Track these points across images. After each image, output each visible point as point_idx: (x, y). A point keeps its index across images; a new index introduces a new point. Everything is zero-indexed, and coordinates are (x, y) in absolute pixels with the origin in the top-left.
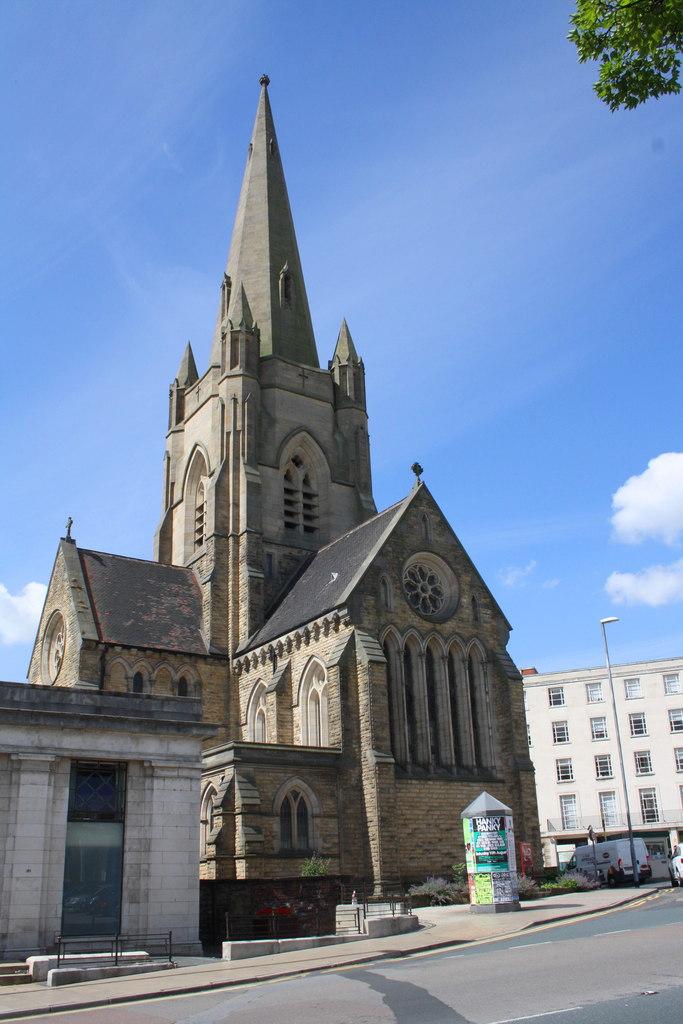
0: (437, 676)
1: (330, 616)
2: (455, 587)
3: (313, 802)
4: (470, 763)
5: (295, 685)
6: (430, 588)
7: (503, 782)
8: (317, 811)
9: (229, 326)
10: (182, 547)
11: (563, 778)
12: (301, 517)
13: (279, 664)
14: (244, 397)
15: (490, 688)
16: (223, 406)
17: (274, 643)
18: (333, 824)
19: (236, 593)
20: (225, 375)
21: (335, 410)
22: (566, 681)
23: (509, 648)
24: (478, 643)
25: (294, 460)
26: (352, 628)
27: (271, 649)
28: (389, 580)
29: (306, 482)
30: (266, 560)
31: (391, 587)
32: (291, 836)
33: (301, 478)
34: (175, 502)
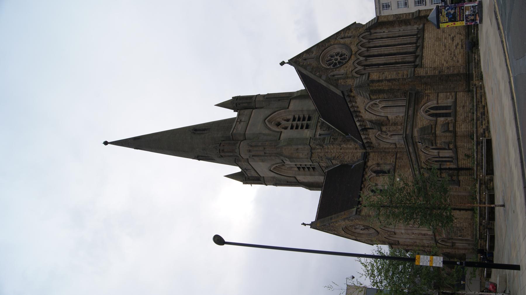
0: (376, 53)
1: (348, 99)
2: (336, 46)
3: (433, 103)
4: (415, 39)
6: (336, 57)
7: (424, 25)
8: (435, 102)
12: (303, 122)
13: (369, 126)
15: (382, 31)
16: (253, 156)
17: (359, 128)
18: (441, 95)
21: (256, 108)
23: (364, 23)
24: (361, 36)
25: (278, 126)
27: (362, 130)
28: (332, 74)
29: (288, 120)
30: (322, 137)
31: (335, 72)
33: (286, 122)
34: (296, 181)
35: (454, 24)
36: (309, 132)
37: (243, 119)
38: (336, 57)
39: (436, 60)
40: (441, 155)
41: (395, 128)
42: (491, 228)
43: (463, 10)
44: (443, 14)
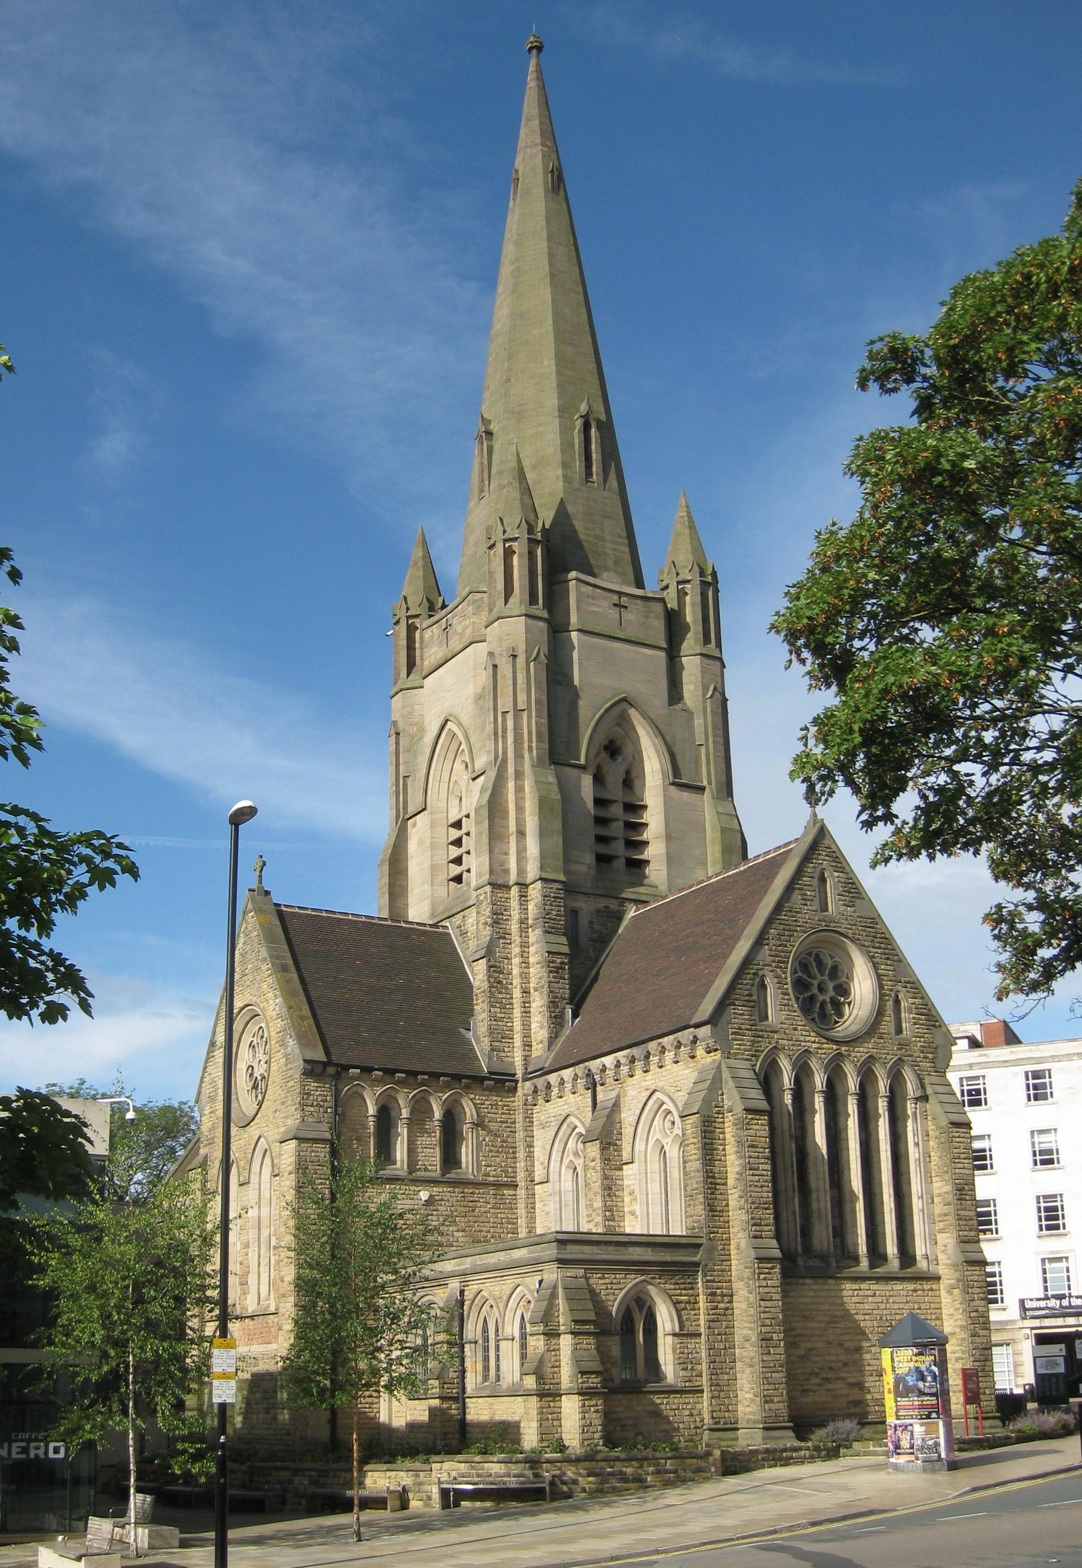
1: (686, 1035)
5: (628, 1131)
6: (830, 986)
9: (500, 529)
10: (427, 888)
11: (1049, 1228)
14: (528, 652)
17: (595, 1065)
19: (525, 977)
20: (495, 614)
22: (1054, 1058)
25: (606, 748)
26: (717, 1055)
27: (589, 1074)
32: (634, 1360)
34: (411, 810)
35: (890, 1392)
36: (583, 868)
37: (628, 616)
38: (830, 986)
39: (813, 1325)
40: (503, 1345)
41: (597, 1186)
42: (284, 1502)
43: (928, 1417)
44: (920, 1358)
